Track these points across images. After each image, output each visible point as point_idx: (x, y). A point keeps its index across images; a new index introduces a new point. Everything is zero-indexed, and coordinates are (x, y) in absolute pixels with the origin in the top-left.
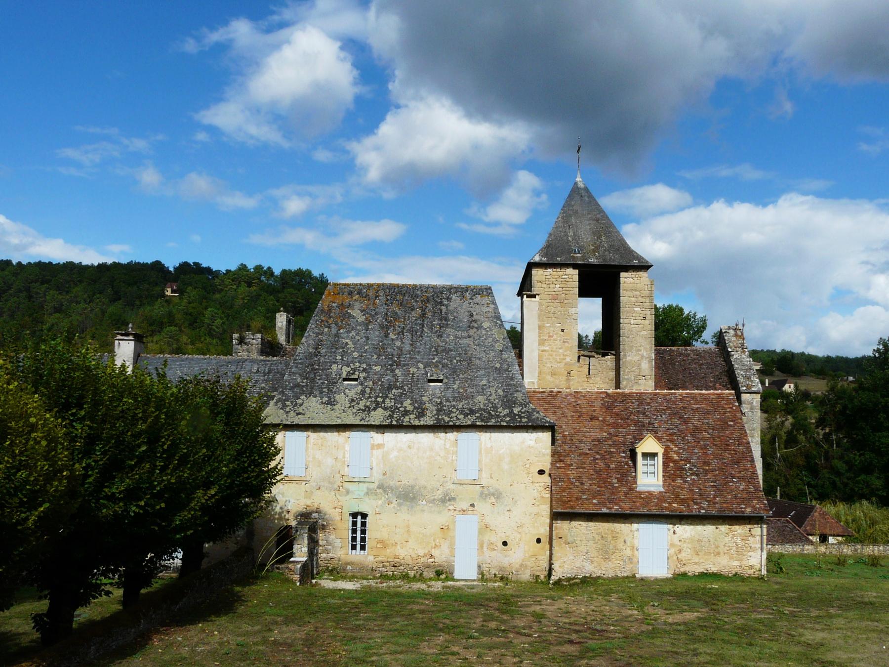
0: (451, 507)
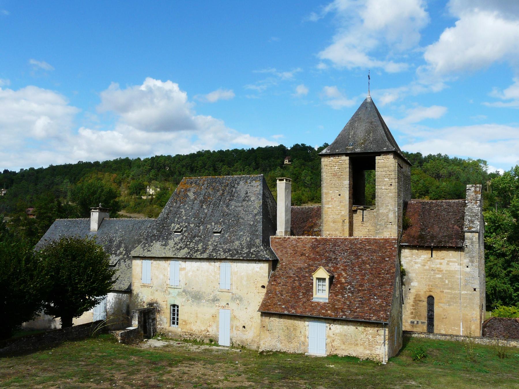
0: (217, 305)
